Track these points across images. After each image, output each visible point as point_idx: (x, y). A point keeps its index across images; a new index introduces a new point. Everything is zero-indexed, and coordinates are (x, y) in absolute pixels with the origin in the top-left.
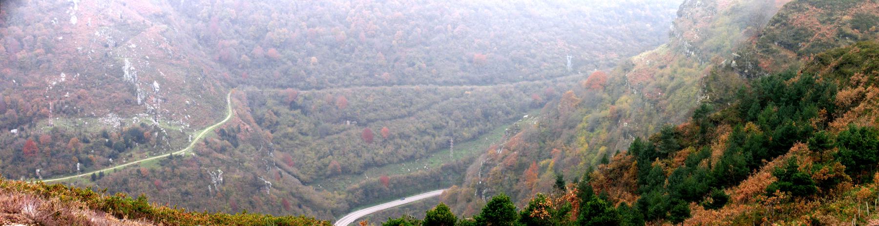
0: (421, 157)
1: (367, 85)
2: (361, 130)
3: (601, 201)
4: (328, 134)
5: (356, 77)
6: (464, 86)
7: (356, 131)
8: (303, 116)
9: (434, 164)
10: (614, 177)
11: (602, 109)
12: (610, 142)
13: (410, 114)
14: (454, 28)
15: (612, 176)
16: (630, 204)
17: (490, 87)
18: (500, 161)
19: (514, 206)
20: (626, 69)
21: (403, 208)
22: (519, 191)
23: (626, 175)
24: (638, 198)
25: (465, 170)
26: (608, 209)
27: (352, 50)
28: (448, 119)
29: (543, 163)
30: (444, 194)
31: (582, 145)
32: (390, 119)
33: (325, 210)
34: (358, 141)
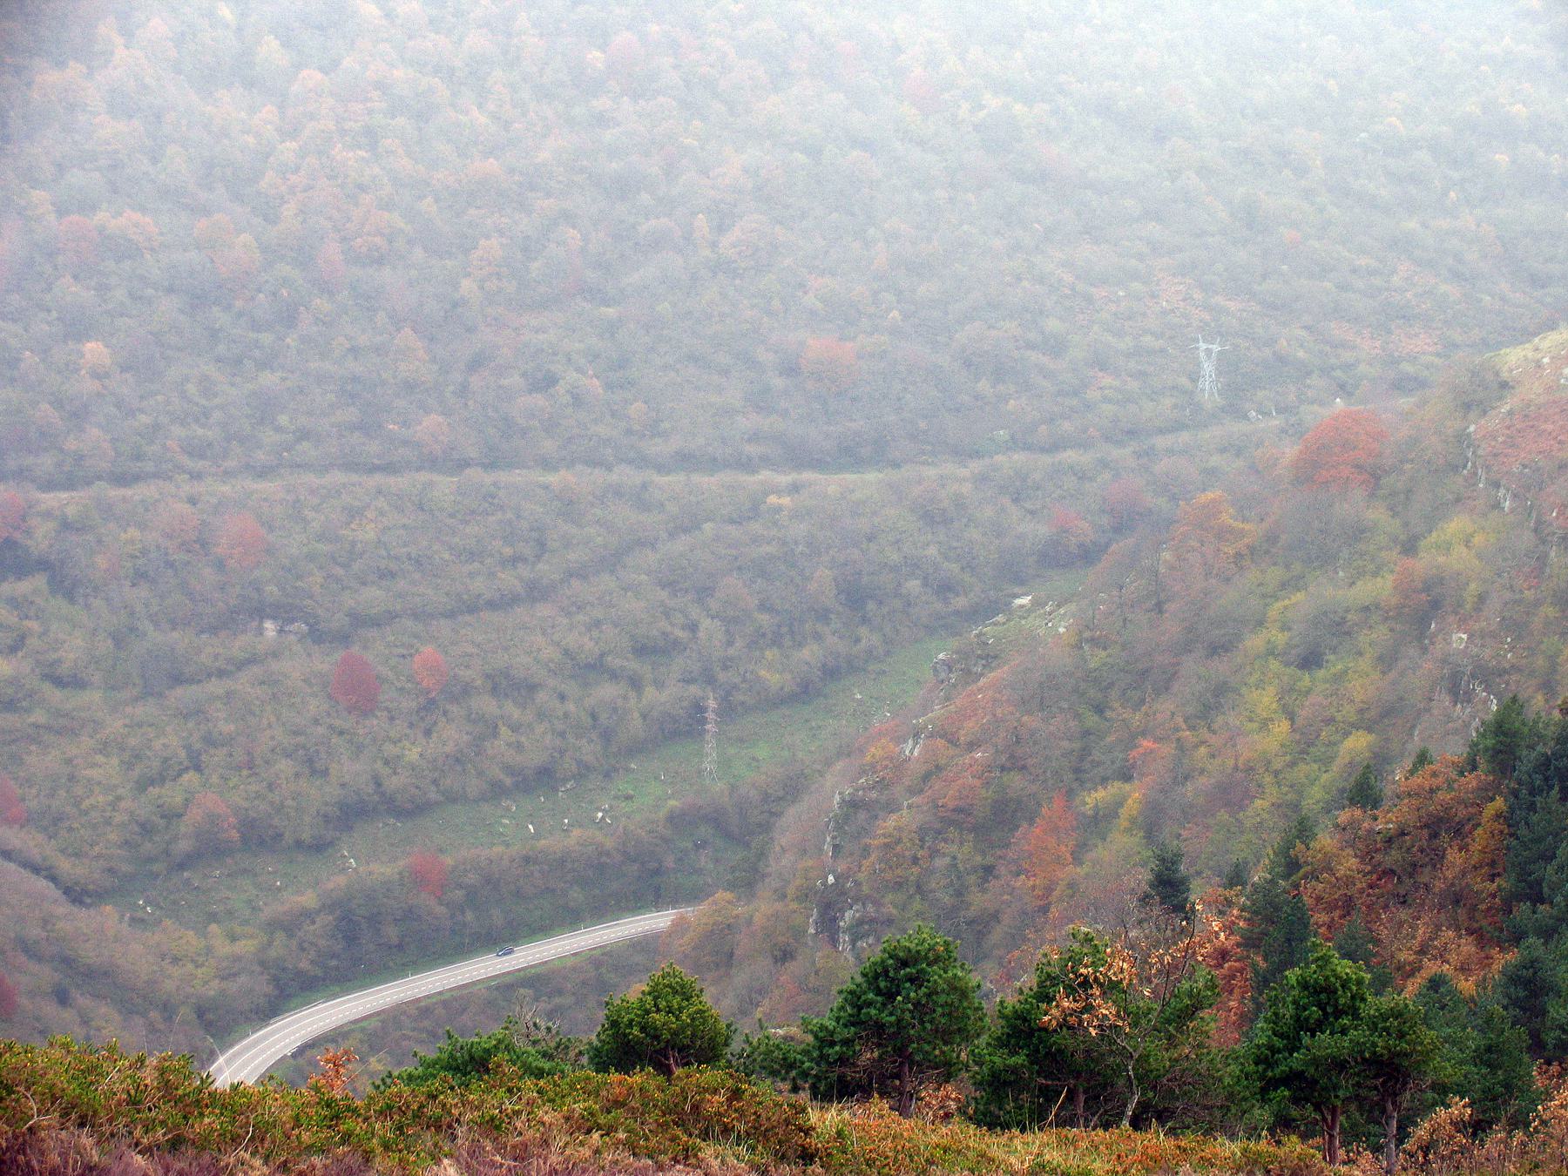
0: (584, 771)
1: (350, 466)
2: (325, 662)
3: (1345, 967)
4: (177, 679)
5: (304, 435)
6: (765, 475)
7: (303, 665)
8: (59, 604)
9: (639, 803)
10: (1401, 865)
11: (1361, 573)
12: (1388, 712)
13: (536, 592)
14: (721, 229)
15: (1392, 858)
16: (1467, 986)
17: (872, 476)
18: (912, 791)
19: (974, 979)
20: (1469, 405)
21: (507, 987)
22: (995, 917)
23: (1454, 857)
24: (1504, 960)
25: (765, 828)
26: (1374, 1004)
27: (289, 318)
28: (695, 612)
29: (1094, 798)
30: (679, 926)
31: (1265, 724)
32: (451, 615)
33: (168, 1009)
34: (315, 706)
